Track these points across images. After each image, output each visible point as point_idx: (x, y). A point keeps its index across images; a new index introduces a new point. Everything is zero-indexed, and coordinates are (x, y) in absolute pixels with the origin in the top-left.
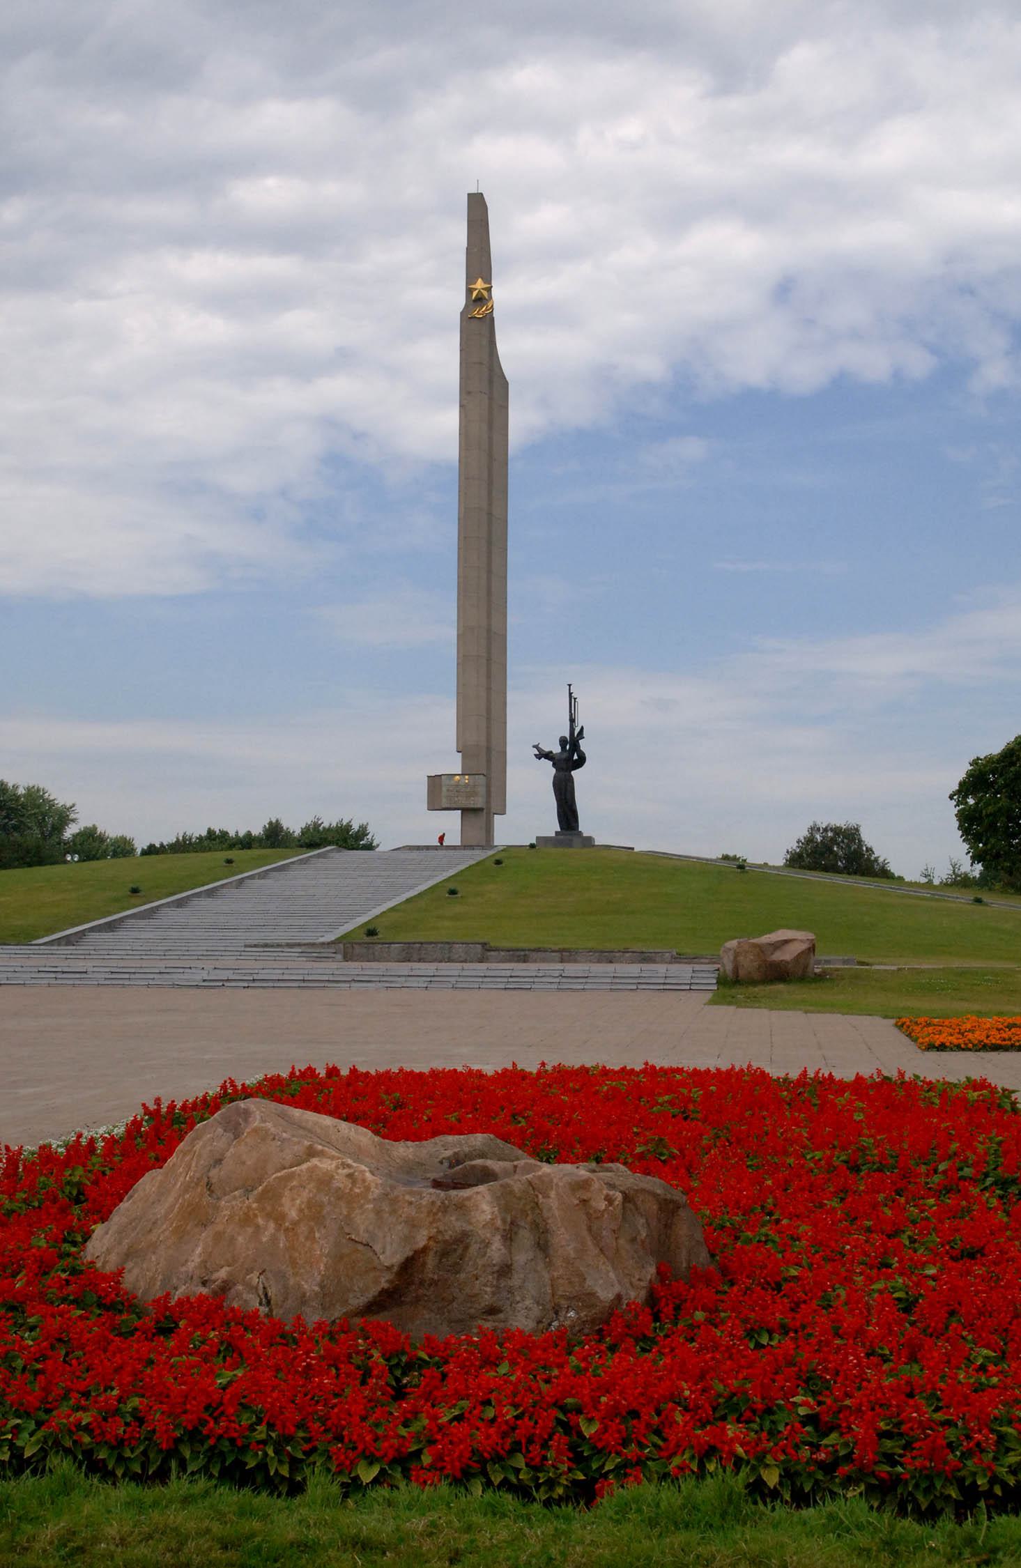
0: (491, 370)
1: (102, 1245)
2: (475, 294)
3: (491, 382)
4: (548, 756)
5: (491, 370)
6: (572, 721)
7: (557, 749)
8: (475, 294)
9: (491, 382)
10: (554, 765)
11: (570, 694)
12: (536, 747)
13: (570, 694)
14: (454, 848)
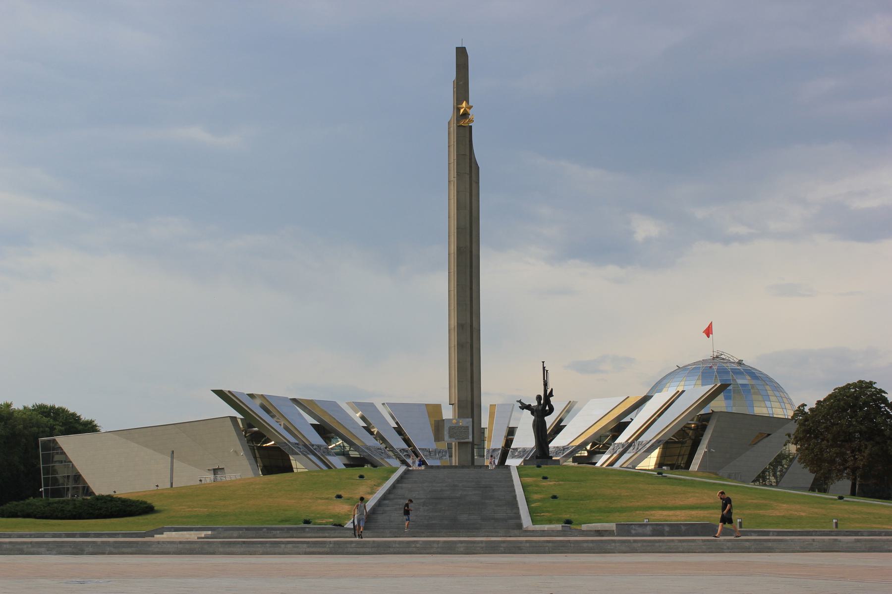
0: (471, 159)
1: (62, 440)
2: (462, 111)
3: (471, 167)
4: (528, 407)
5: (471, 159)
6: (546, 384)
7: (534, 403)
8: (462, 111)
9: (471, 167)
10: (532, 413)
11: (544, 368)
12: (520, 401)
13: (544, 368)
14: (455, 467)
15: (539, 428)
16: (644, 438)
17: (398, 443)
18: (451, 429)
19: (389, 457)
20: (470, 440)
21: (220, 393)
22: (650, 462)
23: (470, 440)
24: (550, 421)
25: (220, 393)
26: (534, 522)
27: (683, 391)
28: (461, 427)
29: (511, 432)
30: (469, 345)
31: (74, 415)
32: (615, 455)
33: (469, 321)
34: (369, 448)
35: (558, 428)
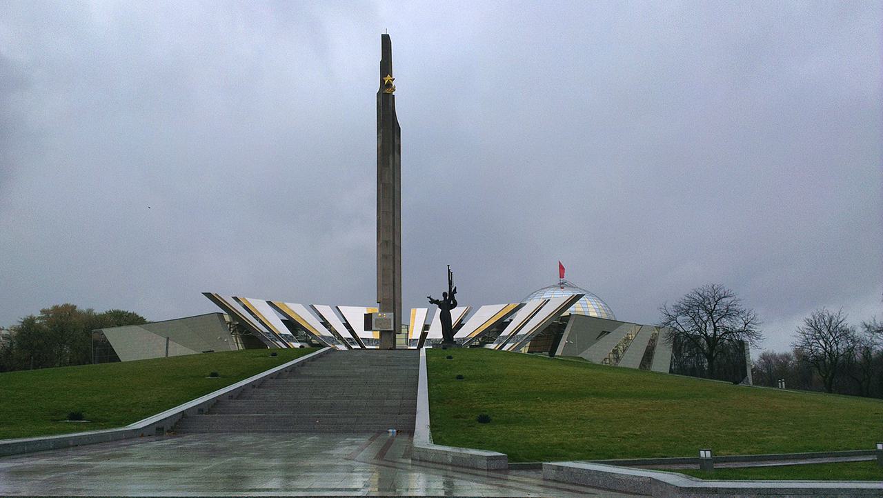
0: (393, 123)
3: (393, 126)
4: (436, 302)
5: (393, 123)
6: (450, 283)
9: (393, 126)
11: (449, 270)
15: (445, 318)
16: (523, 332)
17: (346, 334)
18: (376, 320)
19: (339, 344)
20: (393, 329)
21: (209, 295)
22: (524, 350)
23: (393, 329)
24: (456, 314)
25: (209, 295)
26: (436, 440)
27: (549, 300)
28: (385, 319)
29: (426, 327)
30: (391, 257)
31: (142, 318)
32: (500, 345)
33: (392, 239)
34: (323, 337)
35: (460, 325)
